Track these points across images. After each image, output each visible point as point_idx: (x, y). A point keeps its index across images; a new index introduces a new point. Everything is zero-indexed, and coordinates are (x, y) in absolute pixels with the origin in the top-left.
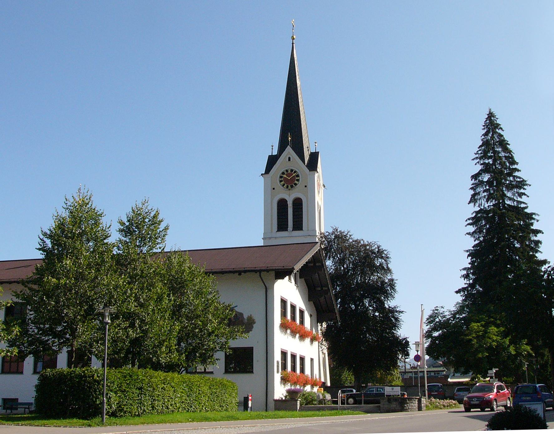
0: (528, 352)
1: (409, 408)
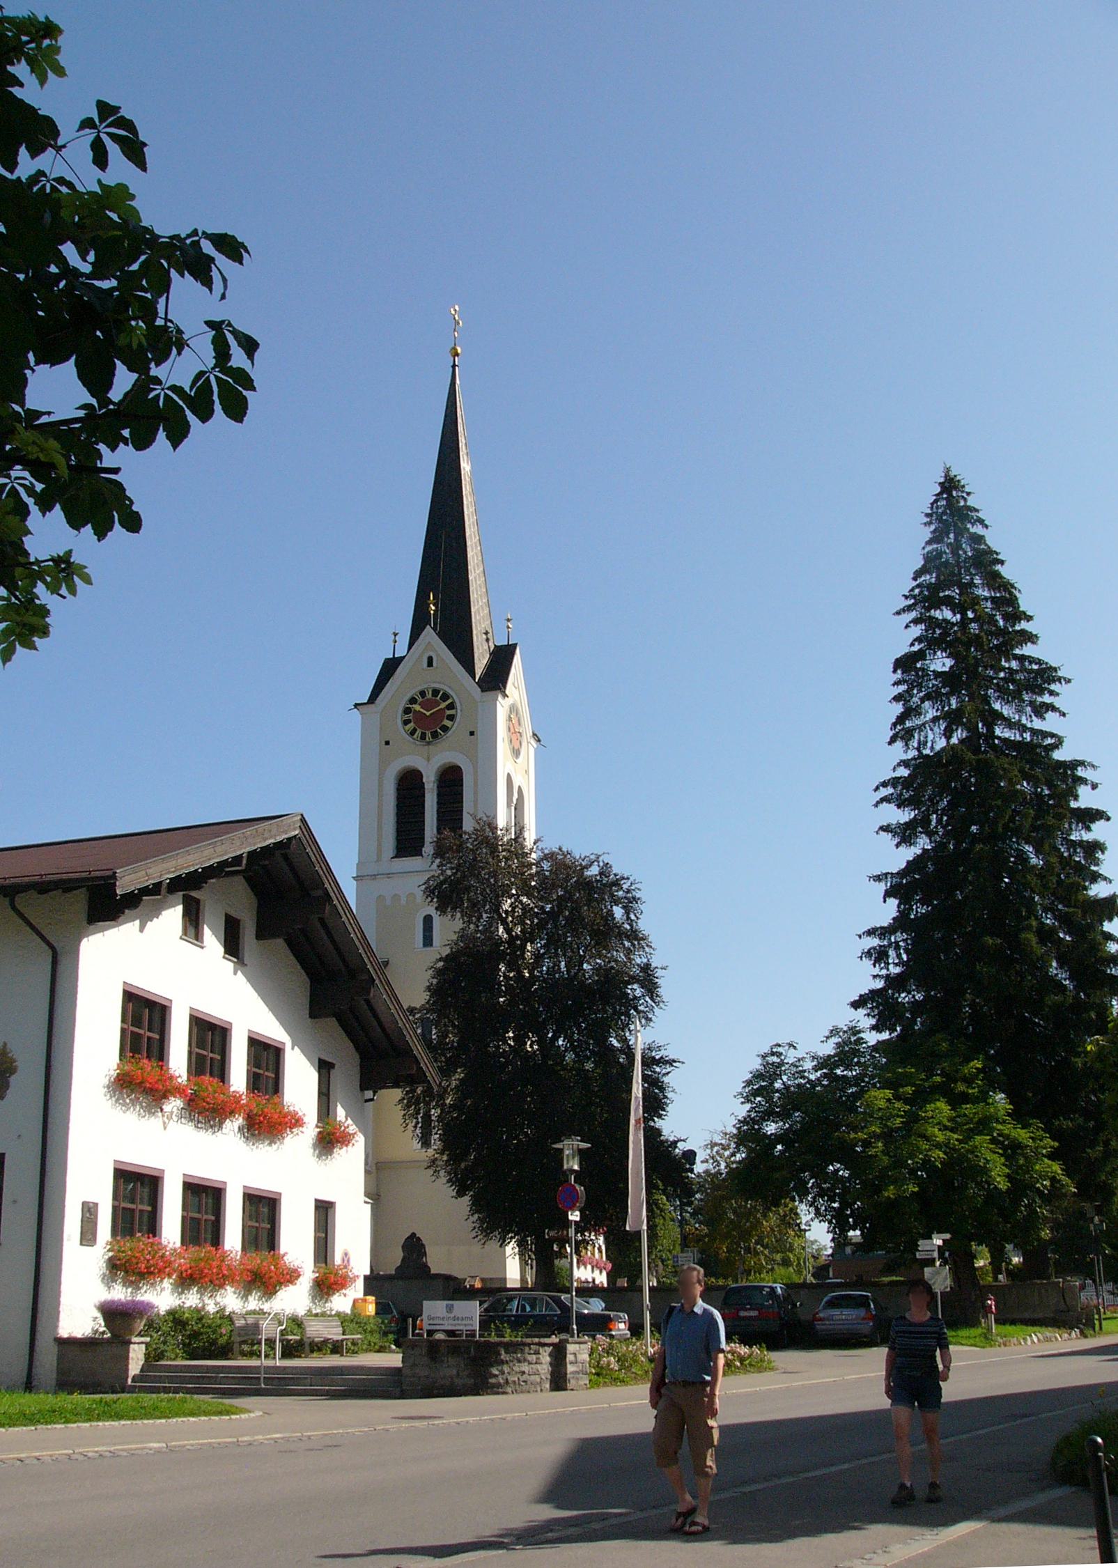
0: (1053, 1180)
1: (507, 1382)
